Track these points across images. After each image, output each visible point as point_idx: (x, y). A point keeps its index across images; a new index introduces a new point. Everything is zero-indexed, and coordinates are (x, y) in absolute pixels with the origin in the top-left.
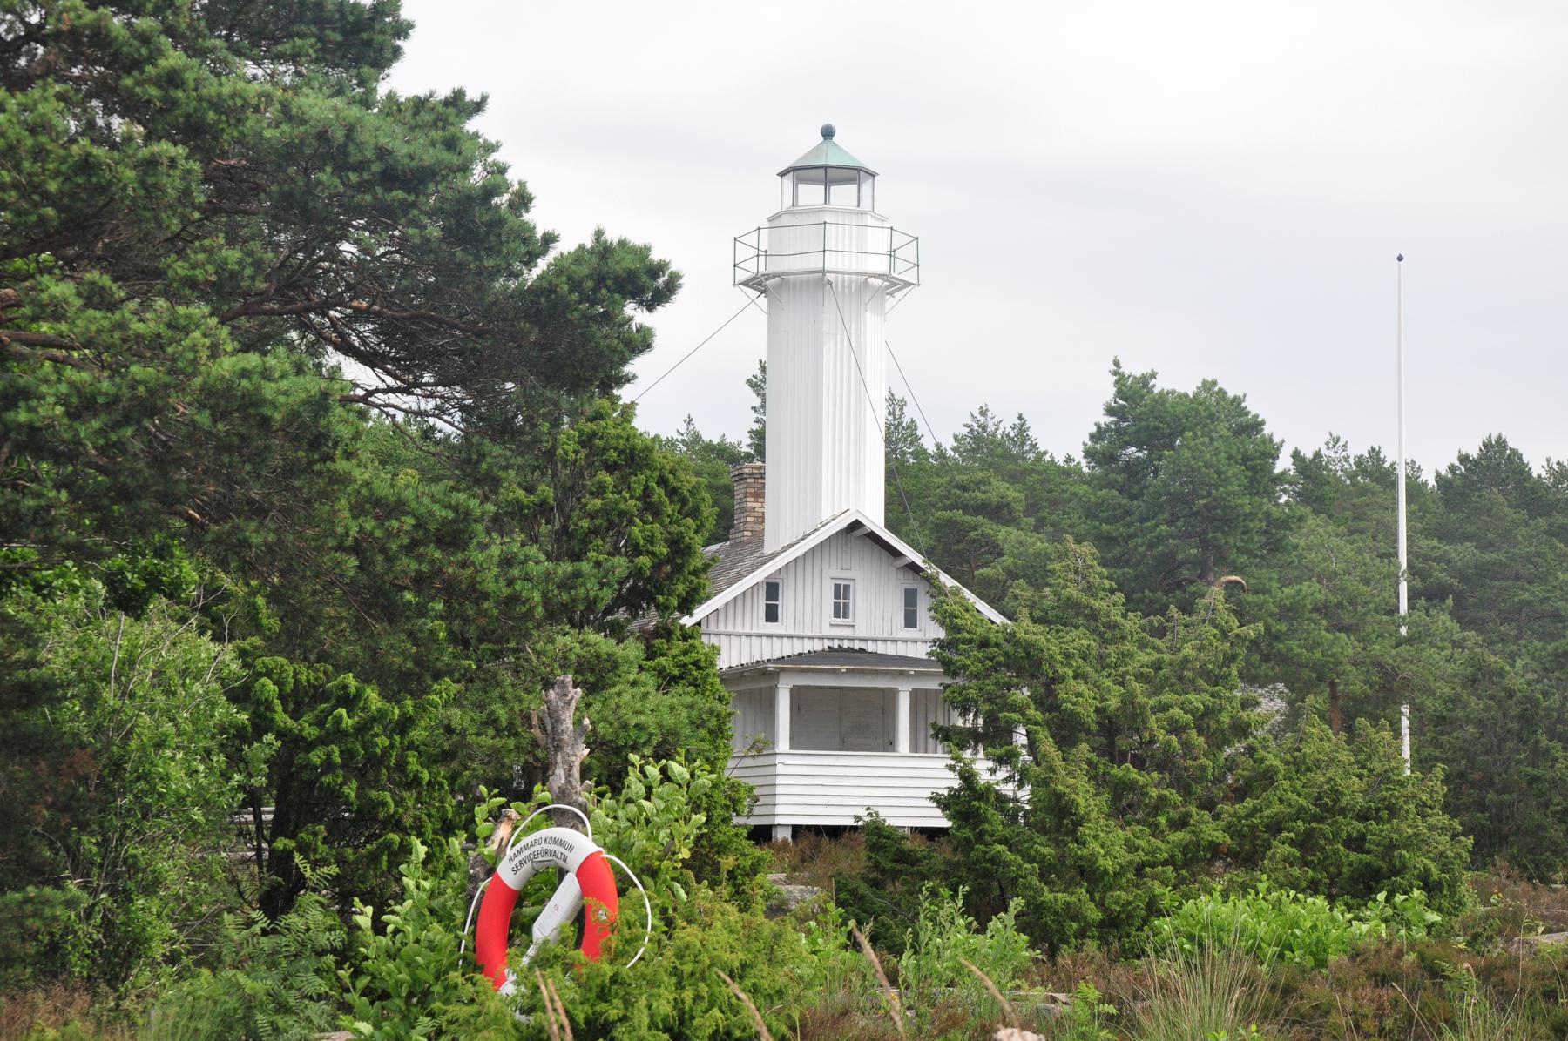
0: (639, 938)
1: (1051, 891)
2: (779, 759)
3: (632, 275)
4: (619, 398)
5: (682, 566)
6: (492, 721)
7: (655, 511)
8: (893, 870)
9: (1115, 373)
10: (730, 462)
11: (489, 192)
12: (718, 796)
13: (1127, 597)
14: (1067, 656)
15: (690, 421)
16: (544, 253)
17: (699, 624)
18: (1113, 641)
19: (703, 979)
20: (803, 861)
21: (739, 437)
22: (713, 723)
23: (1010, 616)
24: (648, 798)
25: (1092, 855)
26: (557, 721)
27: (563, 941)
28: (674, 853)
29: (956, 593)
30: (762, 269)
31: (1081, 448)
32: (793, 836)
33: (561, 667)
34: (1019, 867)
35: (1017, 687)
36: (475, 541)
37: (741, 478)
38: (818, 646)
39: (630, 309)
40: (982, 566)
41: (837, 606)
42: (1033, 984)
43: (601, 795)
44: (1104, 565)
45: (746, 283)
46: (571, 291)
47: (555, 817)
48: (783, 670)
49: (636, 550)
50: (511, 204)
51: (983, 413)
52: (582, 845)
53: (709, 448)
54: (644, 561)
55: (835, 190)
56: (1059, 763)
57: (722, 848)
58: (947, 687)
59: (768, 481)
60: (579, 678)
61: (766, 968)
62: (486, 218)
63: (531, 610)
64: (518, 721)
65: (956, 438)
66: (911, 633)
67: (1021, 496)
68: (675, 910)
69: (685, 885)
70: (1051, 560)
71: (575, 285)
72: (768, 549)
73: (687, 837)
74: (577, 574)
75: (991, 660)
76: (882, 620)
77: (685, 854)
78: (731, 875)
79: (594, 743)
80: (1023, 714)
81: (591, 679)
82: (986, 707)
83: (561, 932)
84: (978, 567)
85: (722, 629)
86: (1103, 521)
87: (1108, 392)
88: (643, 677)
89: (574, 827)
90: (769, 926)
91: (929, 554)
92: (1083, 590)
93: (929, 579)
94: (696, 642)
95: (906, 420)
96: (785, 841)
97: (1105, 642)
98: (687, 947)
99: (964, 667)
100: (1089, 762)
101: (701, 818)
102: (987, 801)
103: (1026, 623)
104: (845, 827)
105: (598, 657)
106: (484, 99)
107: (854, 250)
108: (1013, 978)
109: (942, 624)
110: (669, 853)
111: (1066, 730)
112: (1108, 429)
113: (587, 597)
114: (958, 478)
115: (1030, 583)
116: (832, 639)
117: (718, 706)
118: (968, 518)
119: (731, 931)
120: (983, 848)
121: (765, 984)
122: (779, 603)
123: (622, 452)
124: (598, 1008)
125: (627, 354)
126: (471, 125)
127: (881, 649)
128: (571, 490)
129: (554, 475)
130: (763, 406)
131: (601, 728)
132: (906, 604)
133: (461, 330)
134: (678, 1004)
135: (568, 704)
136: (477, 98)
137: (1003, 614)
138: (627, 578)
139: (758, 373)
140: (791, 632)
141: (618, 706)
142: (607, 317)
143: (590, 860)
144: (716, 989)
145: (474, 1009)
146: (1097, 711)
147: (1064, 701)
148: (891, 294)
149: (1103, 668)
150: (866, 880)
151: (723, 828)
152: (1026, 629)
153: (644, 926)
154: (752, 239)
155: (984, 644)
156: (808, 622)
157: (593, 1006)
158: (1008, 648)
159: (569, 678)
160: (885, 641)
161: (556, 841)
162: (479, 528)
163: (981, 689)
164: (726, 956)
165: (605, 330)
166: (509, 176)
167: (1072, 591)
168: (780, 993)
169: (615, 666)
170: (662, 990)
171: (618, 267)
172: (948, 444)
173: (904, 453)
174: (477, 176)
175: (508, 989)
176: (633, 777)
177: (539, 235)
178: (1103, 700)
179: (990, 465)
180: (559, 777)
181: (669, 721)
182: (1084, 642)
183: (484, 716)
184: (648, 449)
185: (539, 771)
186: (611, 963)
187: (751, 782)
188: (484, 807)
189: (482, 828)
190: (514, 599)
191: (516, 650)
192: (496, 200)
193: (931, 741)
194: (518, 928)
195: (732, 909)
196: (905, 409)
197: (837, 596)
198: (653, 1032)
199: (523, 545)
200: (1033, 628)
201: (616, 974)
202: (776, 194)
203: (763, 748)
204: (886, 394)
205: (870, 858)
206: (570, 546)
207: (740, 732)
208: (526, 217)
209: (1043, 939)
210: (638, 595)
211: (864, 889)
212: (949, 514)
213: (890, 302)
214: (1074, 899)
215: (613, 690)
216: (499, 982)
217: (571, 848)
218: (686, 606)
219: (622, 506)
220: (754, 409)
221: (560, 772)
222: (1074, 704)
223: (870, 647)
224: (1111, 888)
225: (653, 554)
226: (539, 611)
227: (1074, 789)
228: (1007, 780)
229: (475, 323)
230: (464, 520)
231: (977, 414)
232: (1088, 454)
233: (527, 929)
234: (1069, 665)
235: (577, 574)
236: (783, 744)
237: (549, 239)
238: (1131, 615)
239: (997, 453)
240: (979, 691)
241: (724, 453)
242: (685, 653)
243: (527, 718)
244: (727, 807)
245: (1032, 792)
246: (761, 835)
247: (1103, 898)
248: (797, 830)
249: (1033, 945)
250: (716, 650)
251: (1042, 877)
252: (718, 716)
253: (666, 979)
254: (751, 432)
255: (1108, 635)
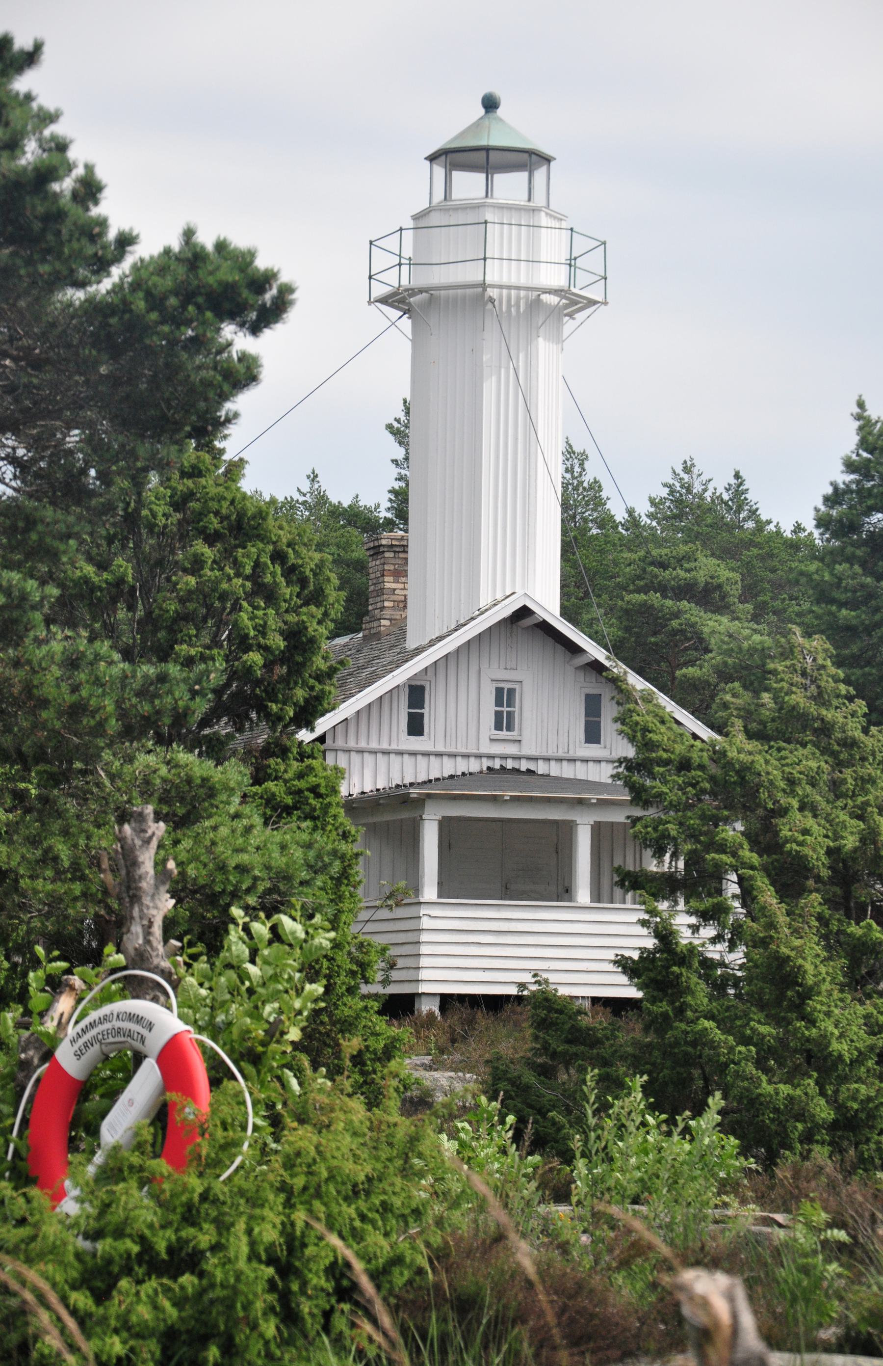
0: (237, 1144)
1: (770, 1082)
2: (423, 911)
3: (229, 289)
4: (222, 451)
5: (303, 665)
6: (49, 858)
7: (271, 596)
8: (566, 1052)
9: (858, 417)
10: (364, 530)
11: (44, 175)
12: (342, 958)
13: (869, 706)
14: (792, 782)
15: (313, 477)
16: (118, 259)
17: (322, 739)
18: (850, 764)
19: (318, 1195)
20: (453, 1041)
21: (376, 498)
22: (336, 868)
23: (718, 728)
24: (253, 961)
25: (824, 1036)
26: (133, 864)
27: (139, 1147)
28: (283, 1033)
29: (648, 699)
30: (405, 282)
31: (812, 514)
32: (442, 1008)
33: (142, 794)
34: (731, 1049)
35: (726, 821)
36: (32, 634)
37: (377, 551)
38: (474, 766)
39: (228, 331)
40: (686, 664)
41: (498, 715)
42: (743, 1202)
43: (194, 957)
44: (838, 664)
45: (384, 300)
46: (150, 310)
47: (135, 987)
48: (429, 796)
49: (243, 643)
50: (75, 195)
51: (687, 469)
52: (166, 1021)
53: (336, 512)
54: (255, 658)
55: (499, 179)
56: (782, 919)
57: (347, 1026)
58: (635, 821)
59: (412, 555)
60: (165, 809)
61: (398, 1181)
62: (40, 209)
63: (101, 724)
64: (84, 862)
65: (652, 502)
66: (593, 751)
67: (736, 576)
68: (285, 1104)
69: (299, 1073)
70: (772, 658)
71: (155, 301)
72: (411, 644)
73: (300, 1013)
74: (162, 678)
75: (694, 786)
76: (560, 740)
77: (294, 1034)
78: (358, 1059)
79: (181, 890)
80: (734, 854)
81: (181, 811)
82: (688, 847)
83: (136, 1134)
84: (680, 666)
85: (352, 744)
86: (842, 605)
87: (847, 442)
88: (247, 809)
89: (155, 999)
90: (404, 1126)
91: (617, 649)
92: (813, 698)
93: (616, 682)
94: (314, 763)
95: (587, 479)
96: (431, 1014)
97: (840, 765)
98: (298, 1154)
99: (660, 795)
100: (820, 918)
101: (318, 989)
102: (690, 967)
103: (740, 738)
104: (508, 997)
105: (189, 781)
106: (38, 47)
107: (523, 259)
108: (719, 1194)
109: (632, 739)
110: (275, 1032)
111: (790, 877)
112: (848, 490)
113: (175, 708)
114: (655, 552)
115: (745, 687)
116: (491, 757)
117: (343, 847)
118: (669, 603)
119: (355, 1134)
120: (683, 1026)
121: (397, 1202)
122: (425, 711)
123: (223, 519)
124: (183, 1234)
125: (226, 387)
126: (22, 84)
127: (554, 770)
128: (156, 566)
129: (137, 546)
130: (407, 459)
131: (191, 871)
132: (587, 715)
133: (15, 359)
134: (288, 1229)
135: (150, 844)
136: (28, 46)
137: (712, 727)
138: (228, 685)
139: (402, 416)
140: (440, 748)
141: (214, 843)
142: (198, 343)
143: (174, 1043)
144: (335, 1209)
145: (24, 1232)
146: (830, 852)
147: (787, 841)
148: (571, 315)
149: (837, 797)
150: (531, 1064)
151: (348, 1000)
152: (740, 747)
153: (244, 1128)
154: (392, 243)
155: (684, 765)
156: (461, 736)
157: (177, 1230)
158: (714, 769)
159: (149, 809)
160: (560, 760)
161: (133, 1017)
162: (38, 616)
163: (681, 824)
164: (349, 1166)
165: (199, 359)
166: (72, 154)
167: (798, 699)
168: (417, 1213)
169: (212, 793)
170: (266, 1212)
171: (211, 280)
172: (643, 509)
173: (585, 520)
174: (31, 152)
175: (70, 1207)
176: (234, 935)
177: (112, 234)
178: (837, 837)
179: (698, 535)
180: (135, 937)
181: (279, 860)
182: (813, 764)
183: (39, 853)
184: (261, 515)
185: (111, 928)
186: (201, 1175)
187: (379, 940)
188: (40, 973)
189: (37, 999)
190: (77, 710)
191: (84, 773)
192: (56, 187)
193: (618, 891)
194: (84, 1127)
195: (357, 1105)
196: (587, 465)
197: (499, 702)
198: (255, 1264)
199: (91, 640)
200: (749, 746)
201: (207, 1190)
202: (419, 186)
203: (403, 896)
204: (561, 447)
205: (536, 1038)
206: (157, 640)
207: (371, 874)
208: (95, 211)
209: (759, 1143)
210: (243, 700)
211: (530, 1078)
212: (643, 597)
213: (569, 325)
214: (798, 1092)
215: (207, 823)
216: (59, 1196)
217: (150, 1026)
218: (307, 715)
219: (225, 586)
220: (395, 462)
221: (137, 929)
222: (801, 844)
223: (541, 768)
224: (845, 1079)
225: (266, 649)
226: (113, 726)
227: (800, 951)
228: (714, 940)
229: (31, 349)
230: (18, 607)
231: (679, 469)
232: (822, 522)
233: (94, 1131)
234: (793, 793)
235: (162, 678)
236: (430, 892)
237: (126, 241)
238: (874, 730)
239: (705, 520)
240: (678, 829)
241: (357, 518)
242: (300, 776)
243: (95, 862)
244: (353, 974)
245: (746, 955)
246: (400, 1006)
247: (836, 1092)
248: (446, 1000)
249: (744, 1152)
250: (339, 774)
251: (760, 1064)
252: (342, 858)
253: (271, 1197)
254: (392, 491)
255: (844, 756)
